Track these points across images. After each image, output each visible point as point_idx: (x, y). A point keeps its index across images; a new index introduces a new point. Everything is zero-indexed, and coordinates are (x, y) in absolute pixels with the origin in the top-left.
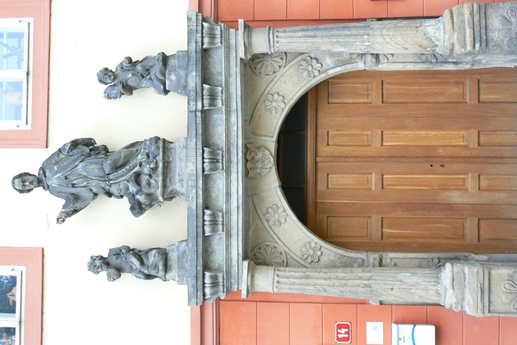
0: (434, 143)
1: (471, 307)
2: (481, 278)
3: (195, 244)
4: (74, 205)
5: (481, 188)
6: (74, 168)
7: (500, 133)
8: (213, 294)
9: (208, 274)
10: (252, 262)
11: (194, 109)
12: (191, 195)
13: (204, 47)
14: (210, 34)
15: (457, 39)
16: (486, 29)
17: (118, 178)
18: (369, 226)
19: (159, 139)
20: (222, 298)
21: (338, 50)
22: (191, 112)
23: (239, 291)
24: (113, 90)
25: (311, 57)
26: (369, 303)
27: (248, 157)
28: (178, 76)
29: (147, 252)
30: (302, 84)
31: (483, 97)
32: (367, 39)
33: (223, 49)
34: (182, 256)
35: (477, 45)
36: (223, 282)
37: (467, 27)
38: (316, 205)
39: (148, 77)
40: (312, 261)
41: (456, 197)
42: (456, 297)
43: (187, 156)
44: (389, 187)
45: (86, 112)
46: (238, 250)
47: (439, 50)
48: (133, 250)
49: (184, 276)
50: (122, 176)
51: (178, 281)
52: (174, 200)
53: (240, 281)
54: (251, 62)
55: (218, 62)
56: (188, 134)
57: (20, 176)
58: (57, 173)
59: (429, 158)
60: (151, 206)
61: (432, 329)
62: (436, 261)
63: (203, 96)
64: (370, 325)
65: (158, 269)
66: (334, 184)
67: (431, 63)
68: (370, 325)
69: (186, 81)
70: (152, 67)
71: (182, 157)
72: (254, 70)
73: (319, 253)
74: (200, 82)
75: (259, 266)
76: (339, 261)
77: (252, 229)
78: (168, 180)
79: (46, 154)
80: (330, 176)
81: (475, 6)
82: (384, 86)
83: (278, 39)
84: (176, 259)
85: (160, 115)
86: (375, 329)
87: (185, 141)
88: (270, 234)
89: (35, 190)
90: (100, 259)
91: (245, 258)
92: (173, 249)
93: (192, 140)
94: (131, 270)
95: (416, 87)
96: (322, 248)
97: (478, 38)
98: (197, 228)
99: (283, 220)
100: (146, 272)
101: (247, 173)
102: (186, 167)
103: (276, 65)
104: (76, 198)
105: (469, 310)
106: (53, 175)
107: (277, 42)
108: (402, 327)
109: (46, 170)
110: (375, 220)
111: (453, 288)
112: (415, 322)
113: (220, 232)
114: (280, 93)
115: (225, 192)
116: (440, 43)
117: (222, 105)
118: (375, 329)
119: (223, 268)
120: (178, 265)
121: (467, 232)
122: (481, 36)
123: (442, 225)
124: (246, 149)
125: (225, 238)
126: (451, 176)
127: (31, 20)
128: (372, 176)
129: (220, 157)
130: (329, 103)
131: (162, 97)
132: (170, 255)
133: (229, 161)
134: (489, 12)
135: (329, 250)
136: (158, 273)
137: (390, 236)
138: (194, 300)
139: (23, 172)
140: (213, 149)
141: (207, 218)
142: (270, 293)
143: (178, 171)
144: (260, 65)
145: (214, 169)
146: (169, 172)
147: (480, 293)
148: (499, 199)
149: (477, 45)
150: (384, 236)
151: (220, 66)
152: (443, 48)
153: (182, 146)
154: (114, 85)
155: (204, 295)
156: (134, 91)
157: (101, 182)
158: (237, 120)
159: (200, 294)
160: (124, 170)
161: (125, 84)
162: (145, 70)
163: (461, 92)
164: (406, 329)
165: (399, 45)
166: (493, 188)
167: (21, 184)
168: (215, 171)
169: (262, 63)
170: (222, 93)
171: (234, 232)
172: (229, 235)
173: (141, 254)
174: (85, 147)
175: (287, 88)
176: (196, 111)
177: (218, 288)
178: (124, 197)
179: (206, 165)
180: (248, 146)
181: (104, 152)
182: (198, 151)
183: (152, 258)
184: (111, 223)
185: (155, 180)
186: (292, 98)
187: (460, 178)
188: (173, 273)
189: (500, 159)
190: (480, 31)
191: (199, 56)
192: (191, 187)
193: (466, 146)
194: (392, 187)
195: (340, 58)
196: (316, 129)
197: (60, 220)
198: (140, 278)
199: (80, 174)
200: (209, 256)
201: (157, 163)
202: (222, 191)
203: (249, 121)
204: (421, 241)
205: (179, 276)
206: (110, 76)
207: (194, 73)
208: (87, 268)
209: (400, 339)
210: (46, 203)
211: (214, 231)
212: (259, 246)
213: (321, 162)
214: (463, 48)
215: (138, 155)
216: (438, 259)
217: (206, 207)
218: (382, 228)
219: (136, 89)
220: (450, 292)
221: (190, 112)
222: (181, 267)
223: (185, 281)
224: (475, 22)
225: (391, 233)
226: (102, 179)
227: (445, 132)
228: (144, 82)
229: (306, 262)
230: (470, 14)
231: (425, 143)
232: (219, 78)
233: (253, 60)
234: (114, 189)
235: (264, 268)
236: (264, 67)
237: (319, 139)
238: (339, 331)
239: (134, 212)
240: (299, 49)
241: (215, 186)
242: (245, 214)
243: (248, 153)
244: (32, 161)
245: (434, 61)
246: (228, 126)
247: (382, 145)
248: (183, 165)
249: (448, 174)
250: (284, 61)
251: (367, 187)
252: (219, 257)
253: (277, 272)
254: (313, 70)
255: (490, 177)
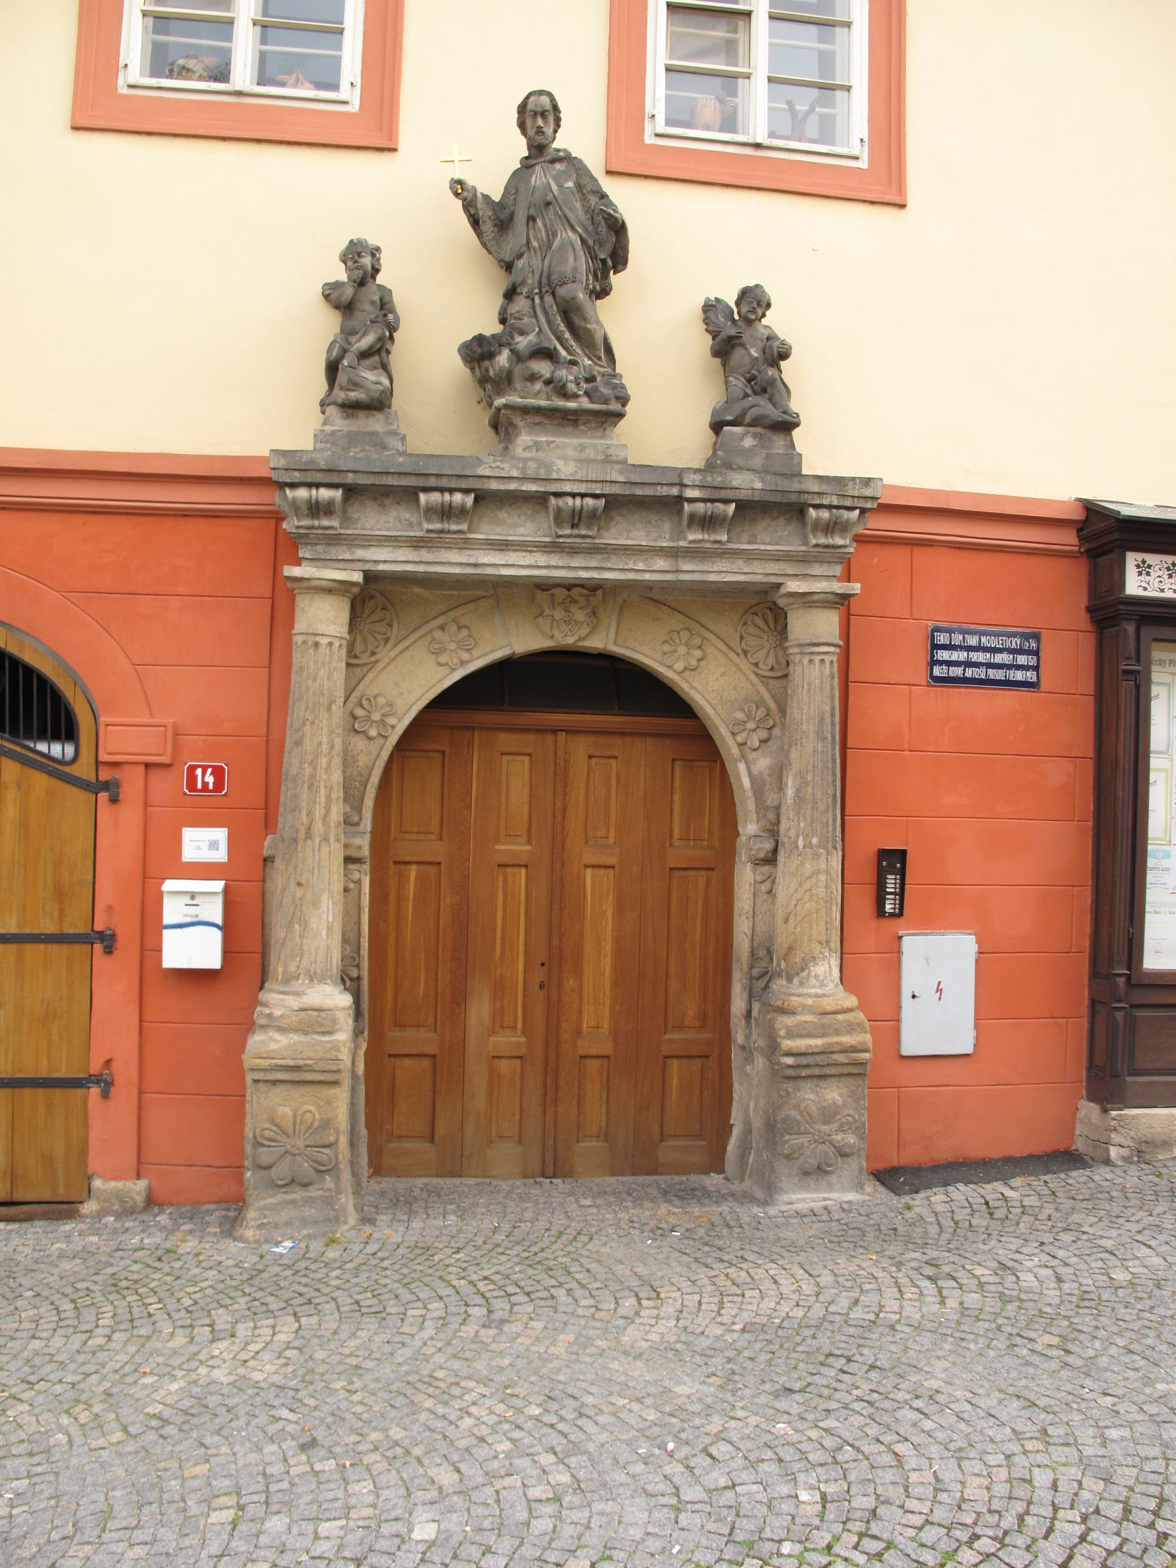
0: (588, 970)
1: (267, 1045)
2: (322, 1066)
3: (403, 470)
4: (492, 220)
5: (496, 1061)
6: (569, 222)
7: (605, 1097)
8: (294, 504)
9: (338, 494)
10: (356, 590)
11: (686, 481)
12: (506, 466)
13: (811, 510)
14: (836, 523)
15: (805, 1022)
16: (820, 1077)
17: (546, 314)
18: (422, 837)
19: (624, 405)
20: (285, 525)
21: (790, 784)
22: (680, 476)
23: (298, 562)
24: (724, 317)
25: (772, 727)
26: (267, 835)
27: (576, 591)
28: (749, 453)
29: (385, 367)
30: (719, 708)
31: (675, 1065)
32: (810, 843)
33: (803, 548)
34: (377, 442)
35: (789, 1061)
36: (319, 528)
37: (826, 1040)
38: (467, 728)
39: (749, 391)
40: (355, 718)
41: (479, 1011)
42: (282, 1016)
43: (588, 461)
44: (501, 878)
45: (684, 253)
46: (385, 562)
47: (779, 984)
48: (391, 338)
49: (334, 443)
50: (549, 322)
51: (322, 431)
52: (490, 432)
53: (320, 564)
54: (767, 605)
55: (775, 537)
56: (634, 465)
57: (555, 108)
58: (560, 186)
59: (557, 960)
60: (483, 381)
61: (214, 961)
62: (354, 973)
63: (712, 501)
64: (220, 834)
65: (349, 390)
66: (511, 767)
67: (751, 968)
68: (220, 834)
69: (740, 468)
70: (770, 400)
71: (587, 451)
72: (752, 610)
73: (373, 732)
74: (741, 497)
75: (349, 605)
76: (355, 773)
77: (426, 593)
78: (538, 419)
79: (595, 166)
80: (526, 759)
81: (866, 1056)
82: (703, 873)
83: (817, 662)
84: (370, 429)
85: (667, 415)
86: (214, 845)
87: (620, 458)
88: (414, 630)
89: (523, 141)
90: (373, 267)
91: (369, 577)
92: (391, 424)
93: (621, 473)
94: (348, 332)
95: (698, 936)
96: (382, 741)
97: (804, 1061)
98: (437, 475)
99: (443, 659)
100: (345, 362)
101: (543, 586)
102: (565, 459)
103: (760, 656)
104: (504, 224)
105: (256, 1041)
106: (555, 178)
107: (811, 661)
108: (218, 903)
109: (565, 164)
110: (437, 849)
111: (303, 1010)
112: (228, 928)
113: (426, 526)
114: (703, 663)
115: (510, 538)
116: (795, 988)
117: (692, 542)
118: (214, 845)
119: (347, 528)
120: (357, 433)
121: (409, 1033)
122: (808, 1066)
123: (422, 984)
124: (593, 588)
125: (412, 534)
126: (520, 1003)
127: (863, 164)
128: (523, 844)
129: (583, 532)
130: (673, 760)
131: (706, 419)
132: (379, 416)
133: (574, 551)
134: (850, 1081)
135: (379, 754)
136: (342, 388)
137: (402, 880)
138: (282, 463)
139: (562, 115)
140: (599, 518)
141: (458, 497)
142: (292, 627)
143: (559, 440)
144: (762, 624)
145: (559, 517)
146: (555, 422)
147: (291, 1062)
148: (473, 1095)
149: (789, 1061)
150: (403, 867)
151: (768, 540)
152: (785, 994)
153: (610, 452)
154: (734, 320)
155: (293, 486)
156: (718, 361)
157: (537, 277)
158: (656, 570)
159: (296, 477)
160: (562, 327)
161: (737, 342)
162: (764, 384)
163: (687, 1023)
164: (214, 911)
165: (796, 906)
166: (496, 1084)
167: (539, 109)
168: (555, 519)
169: (766, 628)
170: (715, 542)
171: (425, 555)
172: (417, 543)
173: (384, 354)
174: (610, 245)
175: (712, 680)
176: (683, 485)
177: (307, 515)
178: (502, 326)
179: (570, 500)
180: (600, 592)
181: (598, 288)
182: (598, 485)
183: (371, 376)
184: (445, 302)
185: (539, 392)
186: (692, 687)
187: (516, 1021)
188: (339, 423)
189: (551, 1095)
190: (817, 1065)
191: (793, 498)
192: (524, 468)
193: (578, 1032)
194: (501, 884)
195: (768, 786)
196: (623, 734)
197: (459, 188)
198: (330, 350)
199: (555, 235)
200: (375, 499)
201: (575, 396)
202: (511, 532)
203: (650, 595)
204: (391, 940)
205: (333, 433)
206: (753, 311)
207: (758, 485)
208: (355, 237)
209: (193, 898)
210: (494, 163)
211: (433, 512)
212: (390, 608)
213: (556, 742)
214: (787, 1033)
215: (590, 359)
216: (359, 978)
217: (481, 497)
218: (418, 863)
219: (724, 365)
220: (293, 1002)
221: (681, 472)
222: (353, 438)
223: (322, 445)
224: (835, 1056)
225: (408, 881)
226: (544, 280)
227: (608, 992)
228: (738, 383)
229: (356, 706)
230: (852, 1047)
231: (588, 950)
232: (745, 537)
233: (771, 610)
234: (520, 304)
235: (345, 615)
236: (757, 632)
237: (602, 740)
238: (210, 770)
239: (474, 343)
240: (795, 704)
241: (523, 518)
242: (458, 581)
243: (585, 592)
244: (581, 136)
245: (755, 972)
246: (646, 551)
247: (586, 866)
248: (570, 452)
249: (524, 996)
250: (767, 674)
251: (502, 833)
252: (373, 520)
253: (337, 643)
254: (746, 732)
255: (518, 1078)
